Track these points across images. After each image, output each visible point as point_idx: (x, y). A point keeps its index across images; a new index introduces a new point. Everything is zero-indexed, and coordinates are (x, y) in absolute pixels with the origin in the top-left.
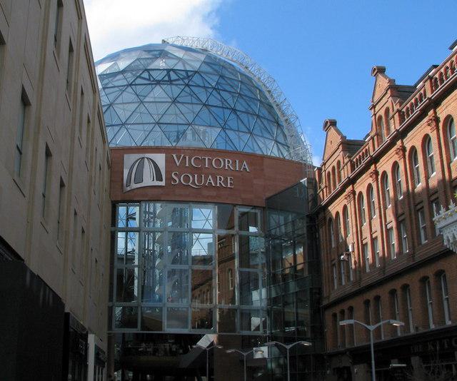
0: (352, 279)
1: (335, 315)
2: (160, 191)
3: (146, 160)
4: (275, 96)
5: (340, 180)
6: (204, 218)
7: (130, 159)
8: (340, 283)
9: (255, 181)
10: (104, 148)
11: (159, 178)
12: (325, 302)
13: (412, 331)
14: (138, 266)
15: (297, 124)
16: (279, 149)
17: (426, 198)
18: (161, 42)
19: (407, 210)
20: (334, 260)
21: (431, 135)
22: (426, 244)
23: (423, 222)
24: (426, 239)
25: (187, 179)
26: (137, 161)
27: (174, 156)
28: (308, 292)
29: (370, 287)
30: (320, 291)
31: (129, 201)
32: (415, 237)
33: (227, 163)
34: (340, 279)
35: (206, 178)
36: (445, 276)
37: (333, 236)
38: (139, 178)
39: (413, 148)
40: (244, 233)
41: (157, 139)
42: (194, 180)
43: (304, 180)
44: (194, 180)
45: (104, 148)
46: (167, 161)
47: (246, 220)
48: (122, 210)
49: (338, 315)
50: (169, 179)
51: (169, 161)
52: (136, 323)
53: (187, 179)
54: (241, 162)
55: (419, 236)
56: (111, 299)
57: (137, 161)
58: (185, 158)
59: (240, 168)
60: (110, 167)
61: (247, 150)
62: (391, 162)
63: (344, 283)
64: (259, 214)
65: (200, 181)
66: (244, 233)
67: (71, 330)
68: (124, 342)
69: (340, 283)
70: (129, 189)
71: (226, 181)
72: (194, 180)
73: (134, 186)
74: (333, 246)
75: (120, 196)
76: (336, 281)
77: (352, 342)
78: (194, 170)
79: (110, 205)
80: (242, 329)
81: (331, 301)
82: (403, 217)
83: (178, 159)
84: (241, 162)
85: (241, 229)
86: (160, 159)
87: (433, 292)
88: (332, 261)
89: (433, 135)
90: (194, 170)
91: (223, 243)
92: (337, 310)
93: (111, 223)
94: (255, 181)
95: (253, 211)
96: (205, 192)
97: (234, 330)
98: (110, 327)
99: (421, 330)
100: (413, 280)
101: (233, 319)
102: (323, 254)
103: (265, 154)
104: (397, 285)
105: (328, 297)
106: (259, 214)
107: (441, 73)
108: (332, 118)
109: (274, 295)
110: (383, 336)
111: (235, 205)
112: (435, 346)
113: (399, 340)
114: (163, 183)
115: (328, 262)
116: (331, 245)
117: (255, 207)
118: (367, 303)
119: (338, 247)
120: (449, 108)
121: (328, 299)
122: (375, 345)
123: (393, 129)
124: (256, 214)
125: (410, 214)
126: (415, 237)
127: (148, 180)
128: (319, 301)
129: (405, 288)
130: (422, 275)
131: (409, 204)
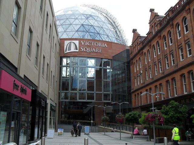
0: (141, 83)
1: (135, 95)
2: (77, 53)
3: (72, 43)
4: (116, 23)
6: (92, 62)
7: (66, 43)
9: (109, 51)
10: (57, 38)
11: (76, 49)
12: (132, 91)
13: (163, 99)
16: (117, 40)
17: (169, 52)
19: (161, 57)
20: (156, 62)
21: (171, 30)
22: (168, 69)
24: (161, 71)
25: (86, 49)
26: (68, 44)
27: (82, 41)
28: (126, 87)
29: (148, 85)
30: (130, 86)
31: (67, 56)
32: (164, 66)
33: (99, 44)
34: (137, 83)
35: (92, 49)
36: (175, 80)
38: (70, 49)
39: (154, 45)
40: (105, 68)
41: (76, 36)
42: (88, 50)
44: (88, 50)
45: (57, 38)
46: (79, 43)
47: (106, 64)
48: (65, 60)
50: (80, 49)
51: (80, 43)
52: (68, 98)
53: (86, 49)
54: (104, 44)
55: (166, 66)
56: (60, 90)
57: (68, 44)
58: (85, 42)
59: (104, 46)
60: (60, 45)
61: (107, 40)
62: (156, 41)
64: (110, 62)
65: (90, 50)
66: (105, 68)
68: (65, 106)
70: (66, 52)
71: (99, 50)
72: (88, 50)
73: (68, 51)
74: (135, 72)
75: (62, 56)
77: (141, 104)
78: (88, 46)
79: (59, 68)
81: (179, 67)
82: (160, 60)
83: (83, 42)
84: (104, 44)
85: (104, 66)
86: (77, 42)
87: (171, 85)
88: (145, 69)
89: (172, 31)
90: (88, 46)
91: (98, 73)
92: (136, 93)
93: (58, 89)
94: (109, 51)
95: (108, 60)
96: (92, 54)
97: (101, 101)
98: (59, 99)
99: (166, 99)
100: (163, 82)
101: (101, 97)
102: (132, 75)
103: (112, 41)
104: (157, 84)
105: (133, 89)
106: (110, 62)
107: (173, 10)
108: (135, 28)
109: (114, 89)
111: (102, 59)
112: (95, 49)
113: (158, 102)
114: (78, 51)
115: (152, 63)
116: (134, 71)
117: (109, 59)
118: (135, 95)
119: (137, 72)
120: (178, 20)
122: (154, 103)
123: (133, 55)
124: (109, 62)
125: (163, 59)
126: (164, 66)
127: (73, 49)
128: (130, 91)
129: (160, 84)
130: (146, 89)
131: (162, 55)
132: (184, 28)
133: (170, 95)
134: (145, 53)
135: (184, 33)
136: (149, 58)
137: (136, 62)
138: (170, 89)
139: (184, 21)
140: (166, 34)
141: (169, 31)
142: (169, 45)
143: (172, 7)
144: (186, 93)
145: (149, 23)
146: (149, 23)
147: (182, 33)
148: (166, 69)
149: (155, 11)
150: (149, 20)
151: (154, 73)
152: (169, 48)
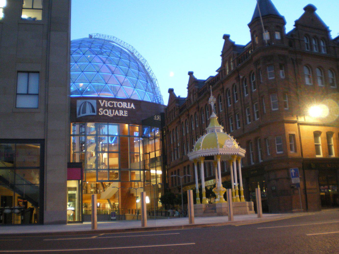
3: (87, 103)
5: (175, 116)
7: (79, 102)
8: (174, 159)
11: (93, 111)
14: (103, 172)
15: (157, 83)
18: (88, 37)
23: (232, 122)
37: (187, 128)
38: (84, 112)
43: (143, 136)
49: (173, 172)
53: (106, 112)
63: (176, 159)
65: (112, 113)
67: (152, 185)
69: (174, 159)
70: (79, 116)
73: (82, 115)
76: (173, 158)
80: (99, 184)
90: (108, 108)
108: (171, 87)
110: (191, 181)
114: (95, 114)
115: (190, 136)
119: (173, 143)
121: (170, 165)
132: (219, 105)
133: (253, 159)
134: (192, 116)
135: (219, 111)
136: (220, 107)
137: (173, 131)
138: (252, 153)
139: (235, 89)
140: (230, 88)
141: (234, 84)
142: (251, 92)
143: (211, 77)
144: (262, 161)
145: (188, 88)
146: (187, 88)
147: (249, 90)
148: (246, 123)
149: (232, 38)
150: (221, 50)
151: (183, 150)
152: (234, 106)
